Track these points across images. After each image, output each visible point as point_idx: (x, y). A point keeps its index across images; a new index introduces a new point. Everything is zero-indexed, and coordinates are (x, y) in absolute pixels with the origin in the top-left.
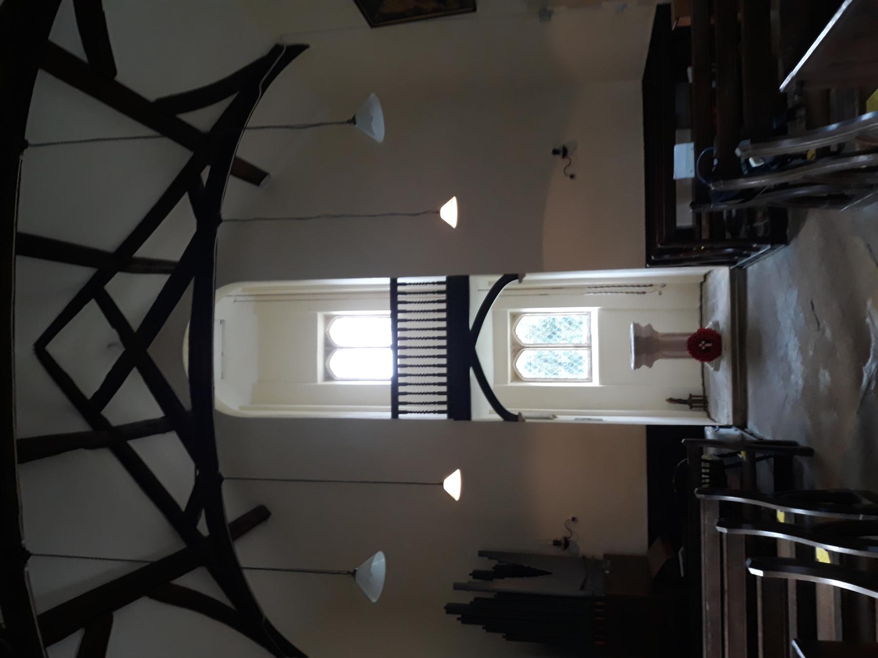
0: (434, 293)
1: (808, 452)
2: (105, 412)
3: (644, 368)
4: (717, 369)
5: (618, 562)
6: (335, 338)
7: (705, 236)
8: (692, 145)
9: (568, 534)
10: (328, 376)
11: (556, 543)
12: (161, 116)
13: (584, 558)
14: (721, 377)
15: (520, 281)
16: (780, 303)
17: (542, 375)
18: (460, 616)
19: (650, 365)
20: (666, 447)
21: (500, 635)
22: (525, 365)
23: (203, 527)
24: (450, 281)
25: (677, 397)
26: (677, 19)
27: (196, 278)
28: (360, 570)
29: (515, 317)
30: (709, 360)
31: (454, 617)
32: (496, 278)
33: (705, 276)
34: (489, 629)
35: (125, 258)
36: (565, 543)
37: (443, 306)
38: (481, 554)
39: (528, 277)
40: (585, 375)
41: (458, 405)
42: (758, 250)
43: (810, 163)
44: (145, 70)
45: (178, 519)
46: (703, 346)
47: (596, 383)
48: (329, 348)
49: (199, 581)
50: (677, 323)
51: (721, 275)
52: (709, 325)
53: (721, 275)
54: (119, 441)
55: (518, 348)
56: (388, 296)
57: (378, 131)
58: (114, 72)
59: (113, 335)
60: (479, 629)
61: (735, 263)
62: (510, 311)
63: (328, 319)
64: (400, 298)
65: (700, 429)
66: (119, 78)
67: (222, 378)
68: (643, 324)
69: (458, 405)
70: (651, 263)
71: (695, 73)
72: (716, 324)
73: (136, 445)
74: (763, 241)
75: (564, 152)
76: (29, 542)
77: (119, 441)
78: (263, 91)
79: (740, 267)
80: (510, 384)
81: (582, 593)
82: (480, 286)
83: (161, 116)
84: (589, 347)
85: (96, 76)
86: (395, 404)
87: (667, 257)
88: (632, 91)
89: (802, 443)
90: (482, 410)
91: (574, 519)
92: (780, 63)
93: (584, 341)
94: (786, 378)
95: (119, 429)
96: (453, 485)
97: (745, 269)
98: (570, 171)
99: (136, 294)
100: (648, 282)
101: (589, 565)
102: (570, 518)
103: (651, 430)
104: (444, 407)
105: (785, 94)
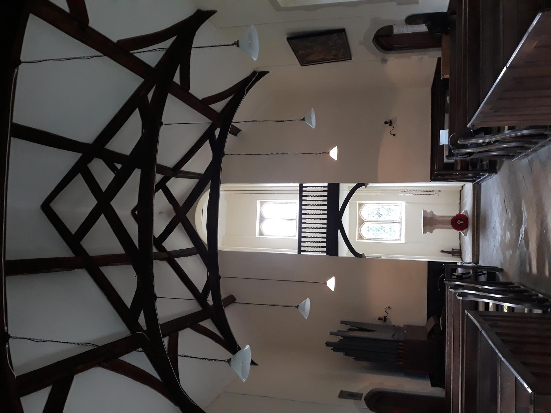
0: (321, 191)
1: (501, 270)
2: (165, 244)
3: (428, 233)
4: (466, 235)
5: (410, 328)
6: (265, 215)
7: (459, 168)
8: (448, 130)
9: (386, 315)
10: (261, 234)
11: (380, 319)
13: (394, 326)
14: (468, 239)
15: (366, 187)
16: (493, 201)
17: (373, 237)
18: (332, 348)
19: (431, 232)
20: (438, 274)
21: (352, 358)
22: (365, 231)
26: (443, 76)
27: (211, 179)
28: (301, 305)
29: (361, 205)
30: (462, 230)
31: (330, 348)
33: (462, 187)
34: (346, 354)
35: (176, 171)
36: (385, 319)
38: (342, 322)
39: (370, 185)
40: (398, 237)
41: (332, 248)
42: (484, 175)
43: (492, 144)
44: (200, 88)
45: (200, 297)
46: (459, 223)
47: (403, 241)
48: (262, 219)
49: (207, 324)
50: (446, 210)
51: (469, 186)
52: (463, 212)
53: (469, 186)
55: (362, 222)
56: (298, 192)
57: (313, 125)
58: (189, 89)
60: (342, 354)
61: (474, 181)
62: (358, 202)
63: (262, 203)
65: (456, 263)
66: (191, 91)
68: (428, 211)
69: (332, 248)
70: (433, 180)
71: (450, 100)
72: (466, 212)
73: (177, 260)
74: (485, 171)
75: (391, 123)
76: (157, 292)
77: (171, 258)
78: (247, 93)
79: (478, 183)
80: (357, 240)
82: (345, 189)
83: (202, 106)
84: (400, 222)
85: (184, 93)
86: (300, 246)
89: (499, 267)
90: (343, 251)
91: (389, 307)
92: (468, 119)
93: (398, 219)
94: (495, 237)
95: (170, 253)
96: (331, 284)
97: (480, 184)
98: (393, 133)
99: (180, 187)
100: (431, 189)
101: (396, 329)
103: (429, 262)
105: (469, 128)
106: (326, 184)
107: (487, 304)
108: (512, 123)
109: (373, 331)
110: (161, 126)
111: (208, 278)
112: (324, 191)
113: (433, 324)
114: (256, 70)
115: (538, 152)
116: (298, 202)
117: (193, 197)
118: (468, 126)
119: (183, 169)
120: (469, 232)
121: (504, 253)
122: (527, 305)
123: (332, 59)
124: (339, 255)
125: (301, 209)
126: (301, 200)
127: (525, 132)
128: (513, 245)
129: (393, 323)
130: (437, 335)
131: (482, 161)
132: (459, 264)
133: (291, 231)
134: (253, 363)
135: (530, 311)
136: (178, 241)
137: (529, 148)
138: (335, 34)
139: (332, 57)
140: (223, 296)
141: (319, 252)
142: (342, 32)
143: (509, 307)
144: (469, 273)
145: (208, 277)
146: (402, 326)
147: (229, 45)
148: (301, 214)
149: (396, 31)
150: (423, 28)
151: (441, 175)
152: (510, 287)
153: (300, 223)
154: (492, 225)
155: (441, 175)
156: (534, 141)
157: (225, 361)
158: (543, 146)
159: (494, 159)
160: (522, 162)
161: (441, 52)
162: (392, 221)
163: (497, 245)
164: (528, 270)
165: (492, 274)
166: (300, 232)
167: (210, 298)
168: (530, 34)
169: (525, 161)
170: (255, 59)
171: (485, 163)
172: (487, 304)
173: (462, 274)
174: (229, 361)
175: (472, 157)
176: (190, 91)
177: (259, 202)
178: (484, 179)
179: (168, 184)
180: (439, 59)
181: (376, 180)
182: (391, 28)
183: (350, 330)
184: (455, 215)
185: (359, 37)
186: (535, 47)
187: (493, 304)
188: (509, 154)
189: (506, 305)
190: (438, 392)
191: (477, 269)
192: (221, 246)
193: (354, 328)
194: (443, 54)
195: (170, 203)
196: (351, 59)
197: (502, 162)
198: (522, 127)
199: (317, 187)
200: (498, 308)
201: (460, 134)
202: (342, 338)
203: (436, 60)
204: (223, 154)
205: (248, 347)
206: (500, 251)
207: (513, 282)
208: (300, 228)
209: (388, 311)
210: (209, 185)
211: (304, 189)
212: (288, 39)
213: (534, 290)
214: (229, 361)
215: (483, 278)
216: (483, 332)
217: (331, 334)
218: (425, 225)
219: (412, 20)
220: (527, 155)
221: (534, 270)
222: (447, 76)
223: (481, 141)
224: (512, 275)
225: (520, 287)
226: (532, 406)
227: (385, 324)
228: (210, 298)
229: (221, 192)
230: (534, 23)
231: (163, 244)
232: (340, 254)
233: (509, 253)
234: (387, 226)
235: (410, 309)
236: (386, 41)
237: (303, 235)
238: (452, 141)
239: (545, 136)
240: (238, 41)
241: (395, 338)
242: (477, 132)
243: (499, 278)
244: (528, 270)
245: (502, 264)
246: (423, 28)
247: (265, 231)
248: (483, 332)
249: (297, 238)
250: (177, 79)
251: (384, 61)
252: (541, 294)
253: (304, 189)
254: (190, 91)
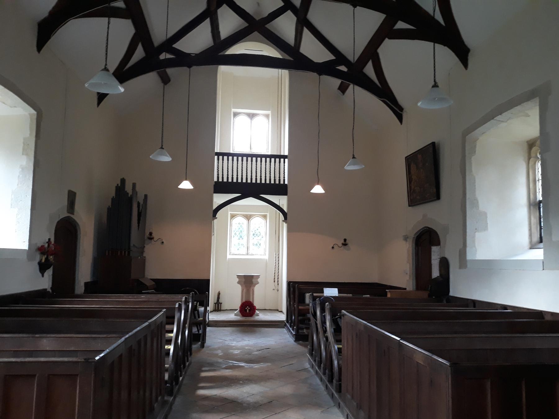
1: (203, 346)
3: (237, 280)
4: (236, 315)
5: (143, 262)
6: (256, 119)
7: (300, 307)
8: (337, 295)
9: (155, 239)
10: (235, 114)
11: (151, 234)
12: (371, 52)
13: (144, 247)
14: (232, 317)
15: (283, 221)
16: (269, 339)
18: (119, 185)
19: (239, 283)
20: (199, 288)
23: (163, 56)
24: (285, 186)
25: (220, 296)
27: (293, 60)
28: (164, 151)
29: (265, 217)
30: (241, 311)
32: (285, 209)
33: (281, 312)
35: (303, 23)
36: (151, 238)
37: (272, 182)
38: (146, 196)
39: (285, 225)
40: (233, 252)
41: (222, 187)
42: (293, 330)
44: (389, 50)
45: (168, 44)
46: (247, 308)
49: (139, 53)
51: (282, 317)
52: (257, 312)
53: (282, 317)
54: (210, 14)
55: (248, 218)
57: (348, 167)
58: (390, 38)
59: (266, 14)
63: (267, 116)
64: (277, 160)
66: (387, 40)
67: (339, 403)
68: (259, 280)
69: (222, 187)
70: (289, 284)
71: (366, 298)
73: (208, 21)
74: (297, 331)
75: (345, 244)
77: (210, 14)
79: (285, 325)
80: (229, 213)
81: (132, 245)
82: (282, 201)
83: (371, 52)
84: (247, 254)
85: (385, 32)
86: (223, 154)
87: (292, 289)
88: (374, 278)
89: (206, 345)
90: (219, 199)
91: (163, 242)
93: (250, 252)
94: (234, 340)
95: (216, 13)
96: (186, 185)
97: (284, 328)
98: (336, 247)
99: (286, 26)
101: (142, 250)
102: (163, 241)
103: (209, 280)
104: (220, 180)
105: (340, 312)
106: (286, 183)
107: (172, 332)
108: (344, 352)
109: (139, 226)
110: (352, 5)
111: (189, 55)
112: (280, 180)
113: (148, 284)
114: (404, 111)
115: (316, 376)
116: (269, 153)
117: (275, 40)
118: (343, 311)
119: (305, 30)
120: (239, 318)
121: (219, 348)
122: (172, 366)
123: (410, 187)
124: (215, 195)
125: (261, 156)
126: (271, 156)
127: (336, 363)
128: (228, 356)
129: (147, 247)
130: (138, 287)
131: (307, 328)
132: (208, 309)
133: (238, 147)
134: (101, 97)
135: (167, 370)
136: (229, 22)
137: (319, 367)
138: (435, 190)
139: (413, 187)
140: (170, 71)
141: (218, 175)
142: (438, 197)
143: (169, 350)
144: (199, 317)
145: (189, 54)
146: (145, 255)
147: (435, 77)
148: (257, 156)
149: (434, 249)
150: (436, 273)
151: (294, 291)
152: (187, 353)
153: (247, 156)
154: (246, 338)
155: (294, 291)
156: (327, 371)
157: (106, 65)
158: (321, 380)
159: (310, 337)
160: (306, 363)
161: (412, 290)
162: (249, 245)
163: (227, 343)
164: (204, 369)
165: (199, 338)
166: (238, 155)
167: (169, 56)
168: (431, 357)
169: (307, 365)
170: (419, 104)
171: (305, 331)
172: (172, 332)
173: (198, 311)
174: (106, 69)
175: (312, 318)
176: (387, 39)
177: (269, 112)
178: (290, 331)
179: (289, 13)
180: (405, 289)
181: (289, 231)
182: (438, 243)
183: (139, 204)
184: (255, 305)
185: (431, 214)
186: (418, 363)
187: (172, 337)
188: (314, 352)
189: (171, 348)
190: (80, 288)
191: (205, 324)
192: (223, 69)
193: (141, 208)
194: (410, 292)
195: (269, 14)
196: (409, 206)
197: (306, 346)
198: (340, 362)
199: (283, 172)
200: (169, 342)
201: (335, 306)
202: (129, 196)
203: (404, 287)
204: (320, 74)
205: (122, 90)
206: (221, 345)
207: (192, 356)
208: (243, 155)
209: (160, 242)
210: (288, 57)
211: (282, 160)
212: (433, 144)
213: (185, 373)
214: (106, 69)
215: (195, 330)
216: (147, 324)
217: (134, 185)
218: (245, 276)
219: (445, 264)
220: (312, 367)
221: (203, 374)
222: (389, 295)
223: (328, 324)
224: (198, 356)
225: (188, 361)
226: (83, 360)
227: (146, 238)
228: (169, 56)
229: (280, 70)
230: (440, 360)
231: (225, 5)
232: (215, 195)
233: (220, 353)
234: (244, 241)
235: (163, 260)
236: (426, 240)
237: (235, 158)
238: (328, 299)
239: (331, 381)
240: (438, 86)
241: (132, 248)
242: (335, 322)
243: (195, 344)
244: (204, 369)
245: (209, 347)
246: (436, 273)
247: (239, 119)
248: (147, 324)
249: (231, 152)
250: (401, 25)
251: (406, 238)
252: (182, 380)
253: (282, 160)
254: (387, 39)
